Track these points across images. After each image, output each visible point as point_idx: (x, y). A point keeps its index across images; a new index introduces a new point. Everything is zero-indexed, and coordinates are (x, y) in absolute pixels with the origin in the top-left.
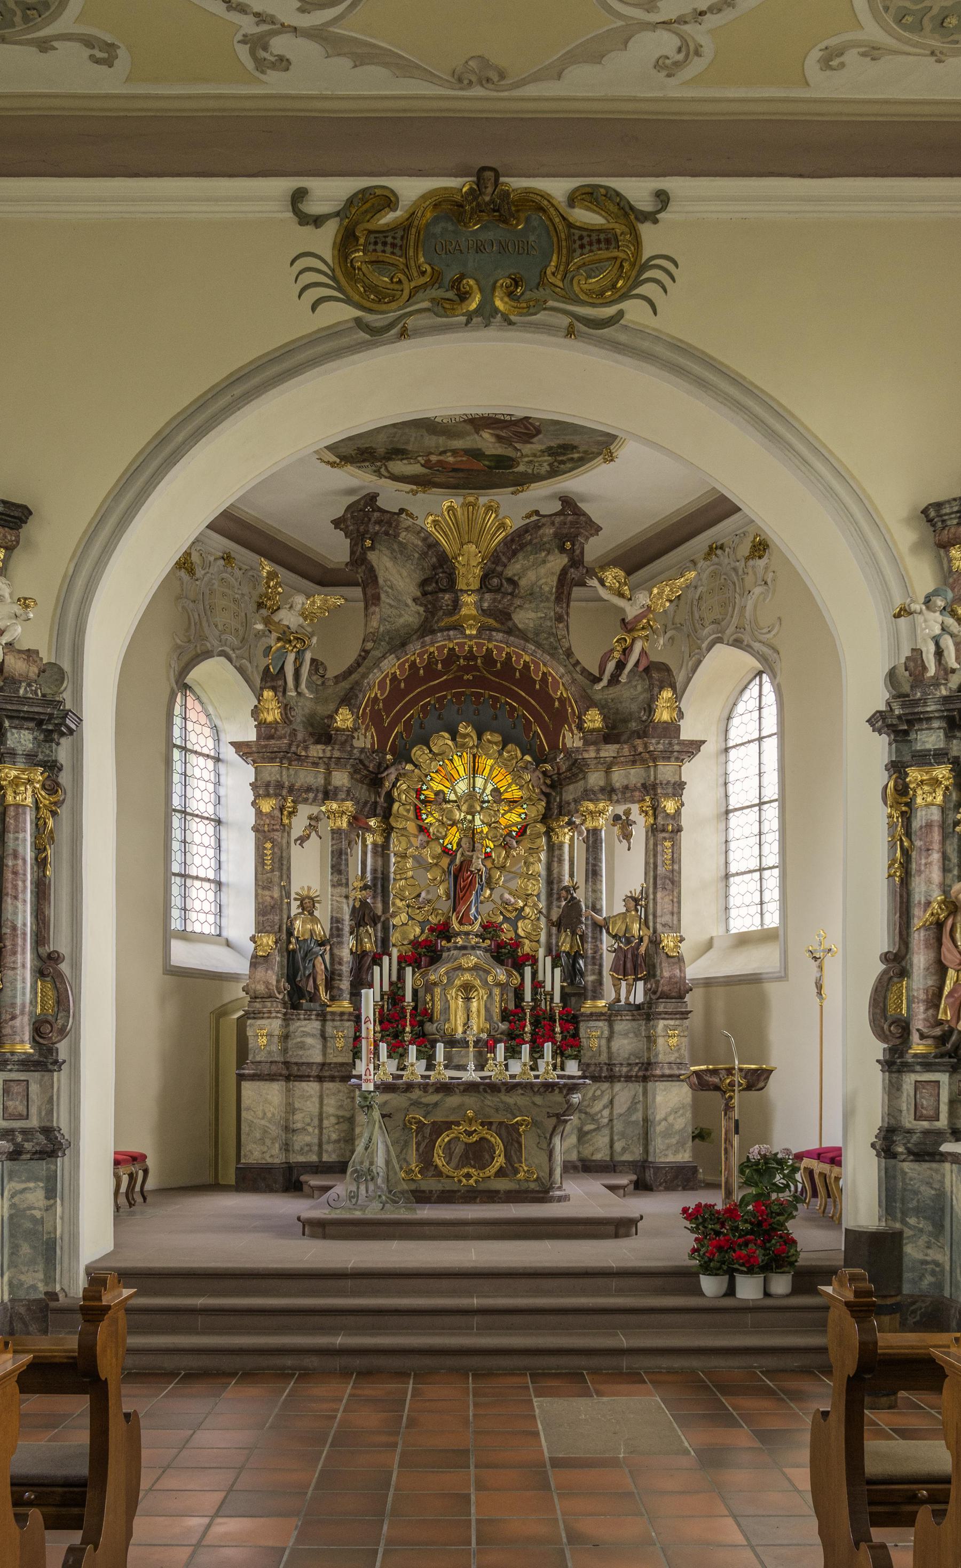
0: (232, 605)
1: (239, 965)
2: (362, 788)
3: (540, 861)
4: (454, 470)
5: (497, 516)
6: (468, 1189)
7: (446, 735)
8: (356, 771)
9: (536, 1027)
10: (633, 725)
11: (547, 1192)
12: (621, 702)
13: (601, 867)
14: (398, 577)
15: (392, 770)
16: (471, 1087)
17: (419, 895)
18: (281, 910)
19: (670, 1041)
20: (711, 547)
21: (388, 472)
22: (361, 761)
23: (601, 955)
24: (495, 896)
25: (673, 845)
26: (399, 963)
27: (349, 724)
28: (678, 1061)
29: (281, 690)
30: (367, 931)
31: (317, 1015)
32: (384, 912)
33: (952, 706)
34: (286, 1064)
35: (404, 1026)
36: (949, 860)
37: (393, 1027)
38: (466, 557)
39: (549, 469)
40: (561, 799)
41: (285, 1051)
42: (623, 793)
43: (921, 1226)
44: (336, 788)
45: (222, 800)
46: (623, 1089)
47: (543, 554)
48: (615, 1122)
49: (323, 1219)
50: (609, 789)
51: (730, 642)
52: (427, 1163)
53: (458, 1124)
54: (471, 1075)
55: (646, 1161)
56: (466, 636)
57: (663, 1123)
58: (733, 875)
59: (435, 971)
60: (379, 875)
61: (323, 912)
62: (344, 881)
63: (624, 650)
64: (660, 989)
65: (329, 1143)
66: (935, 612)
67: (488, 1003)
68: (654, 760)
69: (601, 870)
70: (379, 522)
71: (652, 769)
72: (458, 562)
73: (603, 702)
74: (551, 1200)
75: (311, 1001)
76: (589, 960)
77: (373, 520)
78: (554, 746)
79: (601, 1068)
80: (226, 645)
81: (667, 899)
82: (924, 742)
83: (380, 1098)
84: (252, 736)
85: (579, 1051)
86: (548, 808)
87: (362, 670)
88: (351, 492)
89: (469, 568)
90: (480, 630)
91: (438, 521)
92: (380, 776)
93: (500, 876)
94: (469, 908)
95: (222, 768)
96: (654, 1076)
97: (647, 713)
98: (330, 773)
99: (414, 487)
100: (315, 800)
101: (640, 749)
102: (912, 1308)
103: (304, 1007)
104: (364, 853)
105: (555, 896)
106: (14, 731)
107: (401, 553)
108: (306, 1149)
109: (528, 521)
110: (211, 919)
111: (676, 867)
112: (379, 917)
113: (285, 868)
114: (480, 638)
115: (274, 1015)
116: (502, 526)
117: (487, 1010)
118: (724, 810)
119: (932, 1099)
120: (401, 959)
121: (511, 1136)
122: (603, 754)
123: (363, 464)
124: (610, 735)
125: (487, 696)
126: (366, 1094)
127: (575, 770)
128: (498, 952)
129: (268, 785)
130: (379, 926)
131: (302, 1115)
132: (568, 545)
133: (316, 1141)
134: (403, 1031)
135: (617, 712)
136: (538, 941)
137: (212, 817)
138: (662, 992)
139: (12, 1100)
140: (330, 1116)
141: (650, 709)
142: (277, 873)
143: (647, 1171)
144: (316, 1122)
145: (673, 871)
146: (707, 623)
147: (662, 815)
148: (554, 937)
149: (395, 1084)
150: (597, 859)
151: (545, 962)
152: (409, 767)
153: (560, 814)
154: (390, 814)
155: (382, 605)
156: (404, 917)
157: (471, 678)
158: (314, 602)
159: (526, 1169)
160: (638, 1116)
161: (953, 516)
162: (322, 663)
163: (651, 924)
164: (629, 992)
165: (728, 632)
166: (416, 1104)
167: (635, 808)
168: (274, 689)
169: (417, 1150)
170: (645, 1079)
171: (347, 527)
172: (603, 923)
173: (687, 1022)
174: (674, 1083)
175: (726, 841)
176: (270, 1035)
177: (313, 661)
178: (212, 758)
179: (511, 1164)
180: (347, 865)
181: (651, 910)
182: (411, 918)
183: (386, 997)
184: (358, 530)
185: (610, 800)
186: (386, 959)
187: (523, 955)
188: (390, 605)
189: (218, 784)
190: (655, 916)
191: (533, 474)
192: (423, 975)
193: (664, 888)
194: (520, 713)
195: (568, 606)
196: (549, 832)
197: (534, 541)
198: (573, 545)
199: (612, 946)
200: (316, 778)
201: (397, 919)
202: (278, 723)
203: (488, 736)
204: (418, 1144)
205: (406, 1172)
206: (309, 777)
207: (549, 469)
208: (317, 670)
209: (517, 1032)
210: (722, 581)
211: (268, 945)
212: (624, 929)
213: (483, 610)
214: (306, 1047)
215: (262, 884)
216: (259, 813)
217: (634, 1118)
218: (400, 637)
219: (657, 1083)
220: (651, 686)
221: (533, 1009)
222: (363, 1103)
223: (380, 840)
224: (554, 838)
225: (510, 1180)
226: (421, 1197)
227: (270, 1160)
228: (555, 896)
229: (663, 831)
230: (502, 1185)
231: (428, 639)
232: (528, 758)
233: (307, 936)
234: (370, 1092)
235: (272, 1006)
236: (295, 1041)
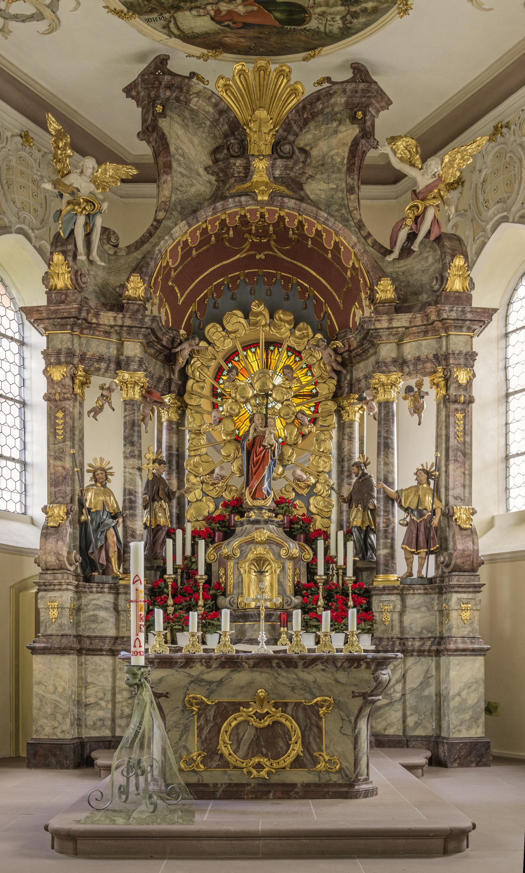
0: (31, 185)
1: (30, 538)
2: (156, 363)
3: (331, 438)
4: (246, 26)
5: (288, 81)
6: (260, 781)
7: (239, 313)
8: (149, 344)
9: (329, 600)
10: (424, 297)
11: (351, 785)
12: (412, 275)
13: (392, 440)
14: (190, 145)
15: (185, 345)
16: (262, 662)
17: (213, 472)
18: (73, 481)
19: (463, 615)
20: (496, 128)
21: (178, 28)
22: (153, 330)
23: (393, 529)
24: (288, 474)
25: (464, 417)
26: (193, 538)
27: (141, 292)
28: (471, 635)
29: (71, 254)
30: (161, 506)
31: (110, 588)
32: (179, 489)
34: (79, 637)
35: (197, 600)
37: (186, 601)
39: (341, 25)
40: (351, 377)
41: (77, 624)
42: (415, 365)
44: (128, 358)
45: (27, 383)
46: (415, 664)
47: (335, 124)
48: (408, 697)
49: (75, 831)
50: (400, 361)
51: (516, 220)
52: (211, 752)
53: (247, 705)
54: (264, 649)
55: (439, 736)
56: (258, 203)
57: (457, 698)
58: (514, 456)
59: (228, 544)
60: (174, 452)
61: (116, 485)
62: (136, 453)
63: (417, 218)
64: (453, 562)
65: (121, 717)
67: (281, 577)
68: (447, 329)
69: (393, 443)
70: (169, 87)
71: (444, 339)
72: (250, 128)
73: (394, 275)
74: (356, 795)
75: (104, 573)
76: (381, 534)
77: (163, 84)
78: (344, 325)
79: (394, 642)
80: (24, 223)
81: (459, 472)
83: (156, 674)
84: (42, 301)
85: (372, 625)
86: (339, 386)
87: (153, 240)
88: (141, 57)
89: (260, 140)
90: (272, 196)
91: (229, 85)
92: (174, 351)
93: (292, 454)
94: (262, 483)
95: (27, 352)
96: (448, 650)
97: (439, 283)
98: (122, 344)
99: (205, 51)
100: (107, 370)
101: (433, 317)
103: (96, 580)
104: (160, 432)
105: (346, 474)
107: (193, 120)
108: (99, 723)
109: (319, 88)
110: (16, 497)
111: (467, 439)
112: (174, 493)
113: (77, 438)
114: (272, 205)
115: (64, 587)
116: (294, 92)
117: (280, 584)
118: (504, 393)
120: (196, 534)
121: (310, 720)
122: (395, 324)
123: (151, 16)
124: (401, 305)
125: (279, 277)
126: (135, 670)
127: (366, 345)
128: (291, 528)
129: (59, 353)
130: (174, 502)
131: (94, 689)
132: (360, 115)
133: (109, 715)
135: (408, 285)
136: (329, 518)
137: (18, 398)
138: (456, 565)
140: (123, 690)
141: (442, 279)
142: (68, 443)
143: (440, 746)
144: (109, 696)
145: (464, 443)
146: (491, 203)
147: (455, 385)
148: (345, 514)
149: (171, 658)
150: (389, 432)
151: (337, 537)
152: (203, 344)
153: (351, 391)
154: (184, 392)
155: (174, 174)
156: (198, 493)
158: (105, 170)
159: (327, 758)
160: (431, 690)
162: (114, 233)
163: (443, 497)
164: (421, 566)
165: (514, 209)
166: (197, 681)
167: (427, 380)
168: (64, 253)
169: (199, 736)
170: (438, 653)
171: (138, 93)
172: (395, 496)
173: (479, 596)
174: (467, 658)
175: (507, 424)
176: (61, 608)
177: (104, 230)
178: (16, 341)
179: (309, 753)
180: (140, 437)
181: (443, 483)
182: (205, 494)
183: (179, 571)
184: (149, 96)
185: (402, 371)
186: (179, 532)
187: (315, 531)
188: (181, 173)
189: (22, 366)
190: (447, 489)
191: (326, 33)
192: (217, 549)
193: (456, 461)
196: (339, 412)
197: (326, 111)
198: (365, 115)
199: (404, 519)
200: (109, 348)
201: (192, 494)
202: (69, 289)
203: (280, 314)
204: (200, 729)
205: (186, 762)
206: (100, 346)
207: (341, 25)
208: (109, 239)
209: (310, 606)
210: (508, 159)
211: (59, 515)
212: (416, 501)
213: (275, 178)
214: (99, 620)
215: (55, 454)
216: (51, 381)
217: (426, 693)
218: (192, 206)
219: (451, 658)
220: (443, 254)
221: (326, 582)
222: (132, 681)
223: (175, 417)
224: (345, 417)
225: (309, 772)
226: (202, 792)
227: (61, 736)
228: (346, 474)
229: (456, 402)
230: (300, 777)
231: (219, 205)
233: (99, 508)
234: (140, 667)
235: (62, 579)
236: (87, 614)
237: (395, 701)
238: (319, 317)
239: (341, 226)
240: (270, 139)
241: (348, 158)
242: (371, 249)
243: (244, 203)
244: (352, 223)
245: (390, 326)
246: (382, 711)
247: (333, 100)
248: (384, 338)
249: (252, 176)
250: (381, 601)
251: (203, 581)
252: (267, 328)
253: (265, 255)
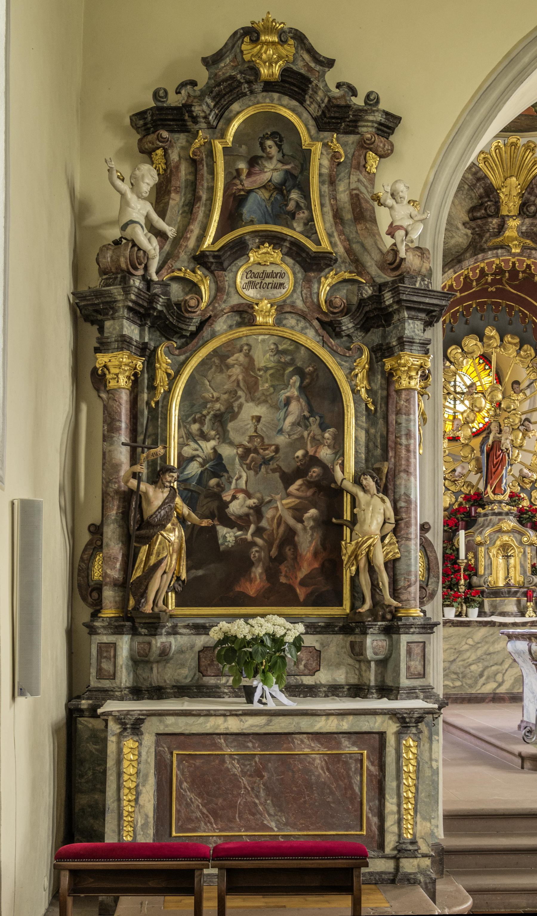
17: (454, 470)
38: (508, 188)
59: (481, 533)
72: (503, 192)
90: (524, 248)
93: (518, 454)
106: (410, 321)
125: (504, 305)
134: (457, 584)
139: (414, 660)
157: (494, 290)
213: (522, 233)
218: (452, 254)
231: (480, 256)
240: (518, 202)
243: (499, 254)
249: (504, 232)
251: (464, 564)
252: (498, 350)
253: (496, 288)
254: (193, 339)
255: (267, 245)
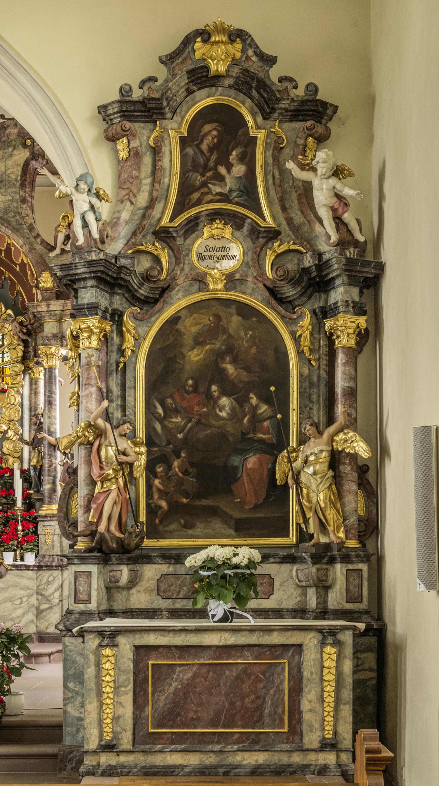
33: (95, 269)
36: (112, 393)
43: (77, 689)
47: (10, 149)
48: (64, 602)
66: (82, 193)
79: (53, 559)
82: (83, 298)
102: (70, 756)
119: (86, 585)
122: (52, 308)
161: (116, 116)
194: (7, 276)
195: (32, 190)
232: (10, 311)
237: (54, 606)
238: (13, 295)
239: (10, 232)
241: (21, 175)
242: (40, 246)
244: (25, 226)
245: (49, 310)
246: (44, 614)
247: (8, 131)
248: (47, 318)
250: (44, 526)
254: (156, 304)
255: (218, 221)
